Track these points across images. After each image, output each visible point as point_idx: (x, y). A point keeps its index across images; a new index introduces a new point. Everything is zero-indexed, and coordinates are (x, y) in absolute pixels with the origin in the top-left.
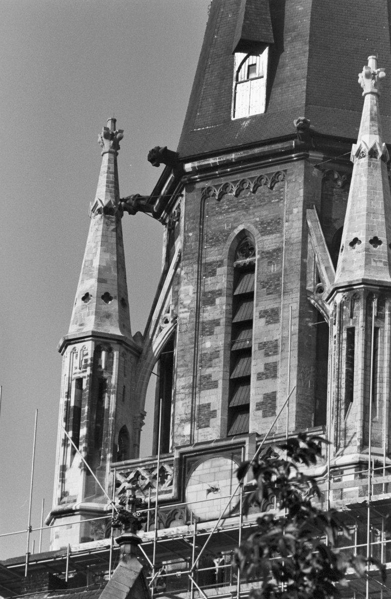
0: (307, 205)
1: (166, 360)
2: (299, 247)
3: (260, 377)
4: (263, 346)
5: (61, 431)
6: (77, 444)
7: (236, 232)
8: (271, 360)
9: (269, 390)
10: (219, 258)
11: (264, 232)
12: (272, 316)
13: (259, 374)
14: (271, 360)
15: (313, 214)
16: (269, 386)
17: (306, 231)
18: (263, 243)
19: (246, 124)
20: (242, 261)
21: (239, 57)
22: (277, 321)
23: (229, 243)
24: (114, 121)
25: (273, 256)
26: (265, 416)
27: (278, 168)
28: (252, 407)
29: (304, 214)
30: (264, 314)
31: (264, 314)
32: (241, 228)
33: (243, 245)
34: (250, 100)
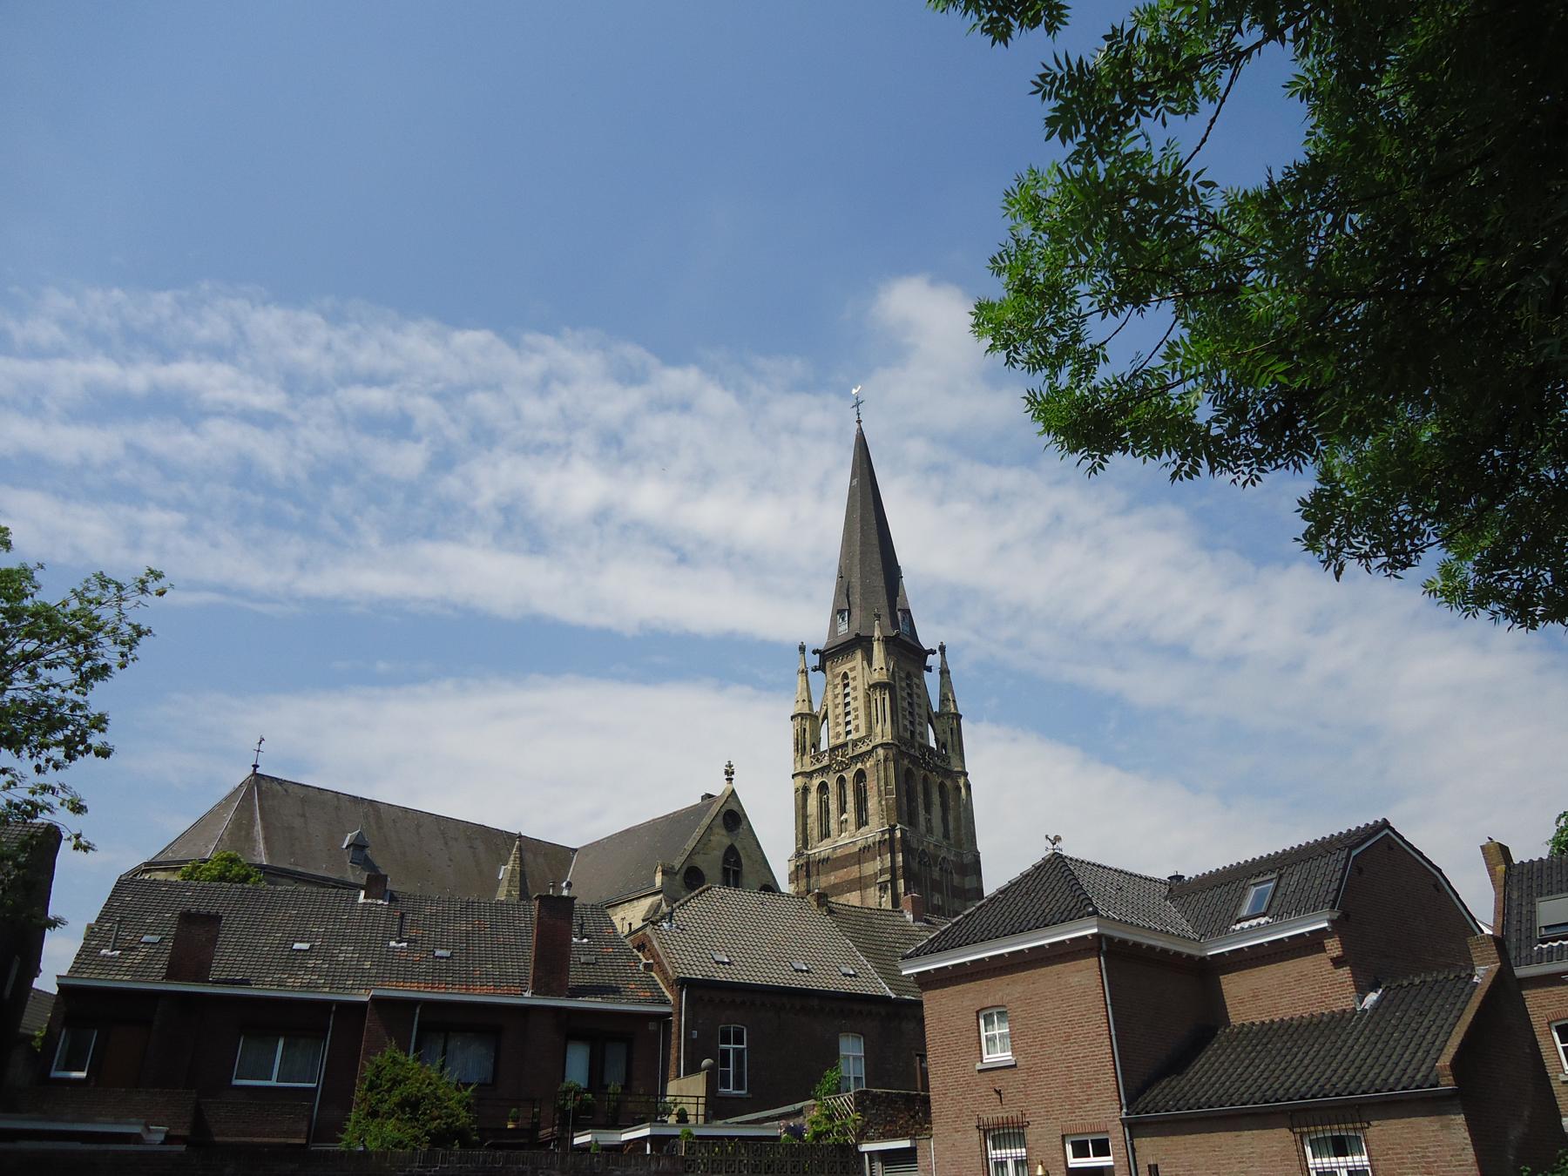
12: (855, 699)
18: (851, 675)
25: (854, 679)
33: (845, 676)
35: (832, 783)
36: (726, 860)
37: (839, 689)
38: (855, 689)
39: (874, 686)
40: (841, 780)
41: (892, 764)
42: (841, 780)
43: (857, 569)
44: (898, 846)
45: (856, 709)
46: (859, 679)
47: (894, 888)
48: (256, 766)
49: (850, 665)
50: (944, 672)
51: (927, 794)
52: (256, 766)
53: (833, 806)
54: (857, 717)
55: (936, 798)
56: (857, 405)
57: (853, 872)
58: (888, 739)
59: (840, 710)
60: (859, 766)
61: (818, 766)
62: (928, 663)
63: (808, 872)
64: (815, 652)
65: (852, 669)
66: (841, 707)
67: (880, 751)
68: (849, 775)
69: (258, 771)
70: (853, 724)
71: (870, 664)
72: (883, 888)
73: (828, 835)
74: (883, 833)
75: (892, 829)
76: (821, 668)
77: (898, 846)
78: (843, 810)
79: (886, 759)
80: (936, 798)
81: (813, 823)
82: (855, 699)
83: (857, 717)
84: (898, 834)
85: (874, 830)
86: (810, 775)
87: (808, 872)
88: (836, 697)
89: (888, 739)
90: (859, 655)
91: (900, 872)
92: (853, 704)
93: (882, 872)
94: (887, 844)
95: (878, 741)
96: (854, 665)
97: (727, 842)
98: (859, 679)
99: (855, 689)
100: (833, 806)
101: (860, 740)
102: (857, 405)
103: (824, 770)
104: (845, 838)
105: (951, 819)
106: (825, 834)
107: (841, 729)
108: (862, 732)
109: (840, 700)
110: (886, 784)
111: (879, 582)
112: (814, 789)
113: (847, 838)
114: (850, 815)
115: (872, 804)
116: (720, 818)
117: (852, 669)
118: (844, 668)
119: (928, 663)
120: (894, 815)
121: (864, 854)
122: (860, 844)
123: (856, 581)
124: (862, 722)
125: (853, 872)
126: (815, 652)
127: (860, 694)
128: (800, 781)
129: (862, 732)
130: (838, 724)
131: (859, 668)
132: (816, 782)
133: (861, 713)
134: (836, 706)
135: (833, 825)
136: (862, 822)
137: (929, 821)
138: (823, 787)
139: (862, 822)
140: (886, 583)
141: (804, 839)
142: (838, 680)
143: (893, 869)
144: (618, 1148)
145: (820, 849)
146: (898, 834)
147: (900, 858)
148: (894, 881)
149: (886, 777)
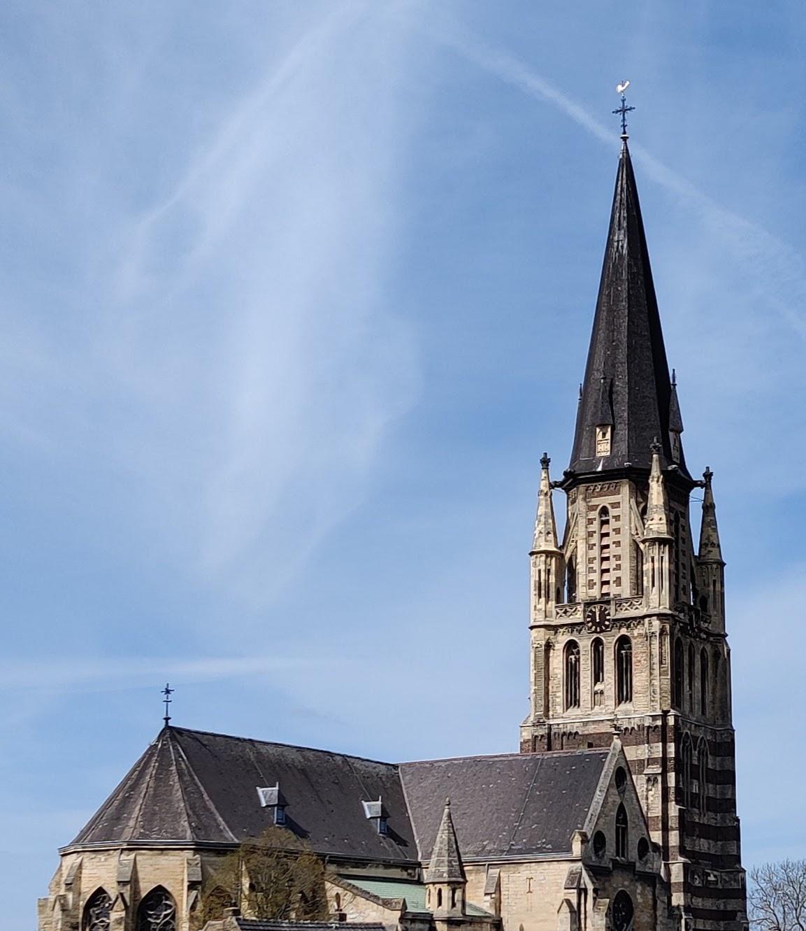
0: (630, 497)
4: (614, 556)
5: (533, 592)
8: (618, 562)
11: (613, 508)
14: (618, 562)
16: (618, 573)
18: (613, 512)
20: (604, 518)
25: (617, 518)
33: (604, 511)
35: (585, 644)
37: (595, 526)
40: (597, 643)
41: (668, 639)
42: (597, 643)
43: (623, 369)
44: (670, 734)
47: (665, 782)
48: (167, 719)
49: (613, 499)
50: (708, 508)
51: (691, 664)
52: (167, 719)
54: (618, 567)
56: (624, 110)
60: (624, 631)
66: (596, 549)
67: (656, 623)
69: (171, 723)
74: (654, 718)
75: (665, 714)
77: (670, 734)
78: (598, 676)
79: (662, 631)
84: (671, 721)
86: (555, 628)
88: (590, 534)
90: (625, 490)
91: (671, 764)
102: (624, 110)
106: (573, 700)
111: (650, 392)
112: (559, 646)
117: (616, 505)
123: (621, 385)
128: (540, 636)
130: (591, 570)
132: (562, 639)
133: (626, 564)
134: (591, 547)
136: (624, 693)
138: (571, 646)
139: (624, 693)
140: (658, 393)
142: (594, 514)
143: (664, 759)
144: (187, 758)
146: (671, 721)
147: (671, 748)
148: (664, 774)
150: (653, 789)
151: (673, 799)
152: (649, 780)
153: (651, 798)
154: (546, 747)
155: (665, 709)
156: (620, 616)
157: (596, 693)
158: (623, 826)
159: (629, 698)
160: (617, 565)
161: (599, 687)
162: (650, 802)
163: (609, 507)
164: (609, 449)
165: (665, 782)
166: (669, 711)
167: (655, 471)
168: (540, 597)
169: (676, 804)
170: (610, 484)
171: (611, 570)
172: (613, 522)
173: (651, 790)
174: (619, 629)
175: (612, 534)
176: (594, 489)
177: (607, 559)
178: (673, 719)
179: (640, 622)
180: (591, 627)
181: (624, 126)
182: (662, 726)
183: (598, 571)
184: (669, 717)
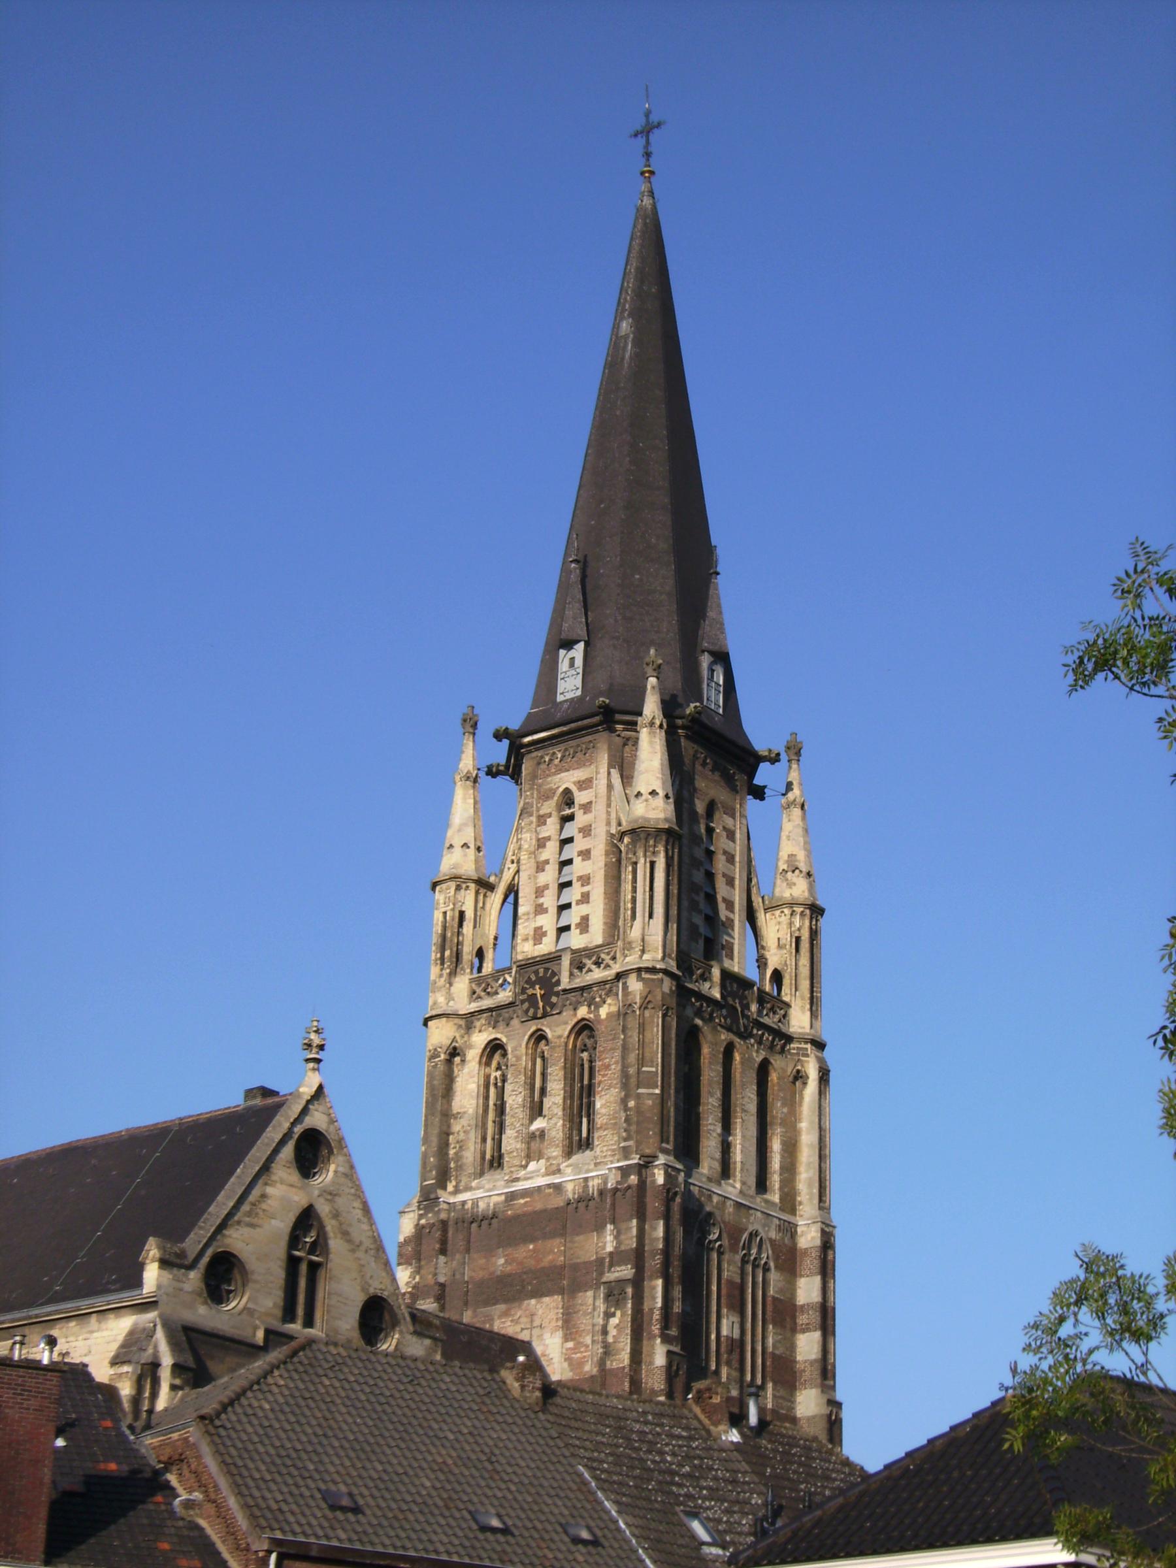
0: (610, 766)
1: (512, 891)
2: (303, 1102)
3: (578, 903)
4: (580, 878)
5: (434, 955)
6: (442, 963)
7: (561, 789)
8: (586, 889)
9: (584, 914)
10: (548, 811)
11: (581, 789)
12: (586, 854)
13: (778, 761)
14: (586, 889)
15: (615, 773)
16: (583, 910)
17: (610, 787)
18: (581, 797)
19: (566, 706)
20: (568, 812)
21: (562, 652)
22: (589, 858)
23: (556, 798)
24: (471, 724)
25: (586, 808)
26: (581, 933)
27: (589, 738)
28: (573, 927)
29: (609, 773)
30: (580, 853)
31: (580, 853)
32: (564, 787)
33: (568, 799)
34: (569, 686)
36: (294, 1240)
38: (586, 831)
39: (639, 834)
45: (585, 880)
46: (600, 808)
47: (638, 1298)
53: (515, 1098)
55: (746, 1099)
56: (648, 130)
57: (554, 1251)
58: (654, 956)
59: (549, 876)
60: (583, 1012)
61: (487, 1003)
62: (758, 780)
63: (444, 1242)
64: (498, 736)
65: (584, 785)
67: (635, 986)
68: (559, 1029)
70: (580, 843)
71: (627, 778)
72: (614, 1295)
73: (496, 1162)
74: (625, 1171)
76: (512, 770)
77: (654, 1204)
78: (537, 1110)
80: (746, 1099)
81: (465, 1131)
82: (586, 854)
83: (585, 898)
85: (600, 1167)
87: (444, 1242)
88: (541, 843)
89: (654, 956)
91: (654, 1262)
92: (579, 867)
93: (616, 1258)
94: (630, 1198)
95: (632, 960)
96: (588, 776)
97: (300, 1200)
98: (600, 808)
99: (586, 831)
100: (515, 1098)
101: (588, 952)
102: (648, 130)
103: (496, 1014)
104: (535, 1176)
105: (776, 1145)
107: (548, 921)
108: (596, 935)
109: (550, 852)
110: (641, 1061)
113: (548, 1174)
114: (553, 1123)
115: (605, 1103)
116: (288, 1151)
117: (584, 785)
118: (567, 780)
119: (758, 780)
120: (653, 1133)
121: (588, 1209)
122: (570, 1190)
124: (596, 911)
125: (554, 1251)
126: (498, 736)
127: (598, 845)
129: (596, 935)
130: (540, 910)
131: (601, 783)
132: (480, 1039)
134: (540, 867)
135: (511, 1142)
137: (726, 1148)
139: (578, 1143)
141: (442, 1169)
142: (549, 807)
143: (638, 1257)
145: (483, 1194)
148: (638, 1282)
149: (642, 1044)
150: (618, 1313)
151: (657, 1332)
152: (608, 1296)
153: (612, 1332)
154: (437, 1246)
155: (648, 1151)
156: (578, 982)
157: (532, 1136)
158: (297, 1253)
159: (586, 1144)
160: (583, 895)
161: (539, 1124)
162: (610, 1339)
163: (574, 789)
164: (580, 685)
165: (638, 1298)
166: (656, 1157)
167: (651, 707)
168: (442, 963)
169: (663, 1342)
170: (578, 746)
171: (573, 904)
172: (581, 819)
173: (613, 1315)
174: (575, 1009)
175: (578, 838)
176: (551, 760)
177: (569, 884)
178: (662, 1172)
179: (610, 990)
180: (527, 1011)
181: (648, 155)
182: (638, 1185)
183: (553, 911)
184: (656, 1171)
